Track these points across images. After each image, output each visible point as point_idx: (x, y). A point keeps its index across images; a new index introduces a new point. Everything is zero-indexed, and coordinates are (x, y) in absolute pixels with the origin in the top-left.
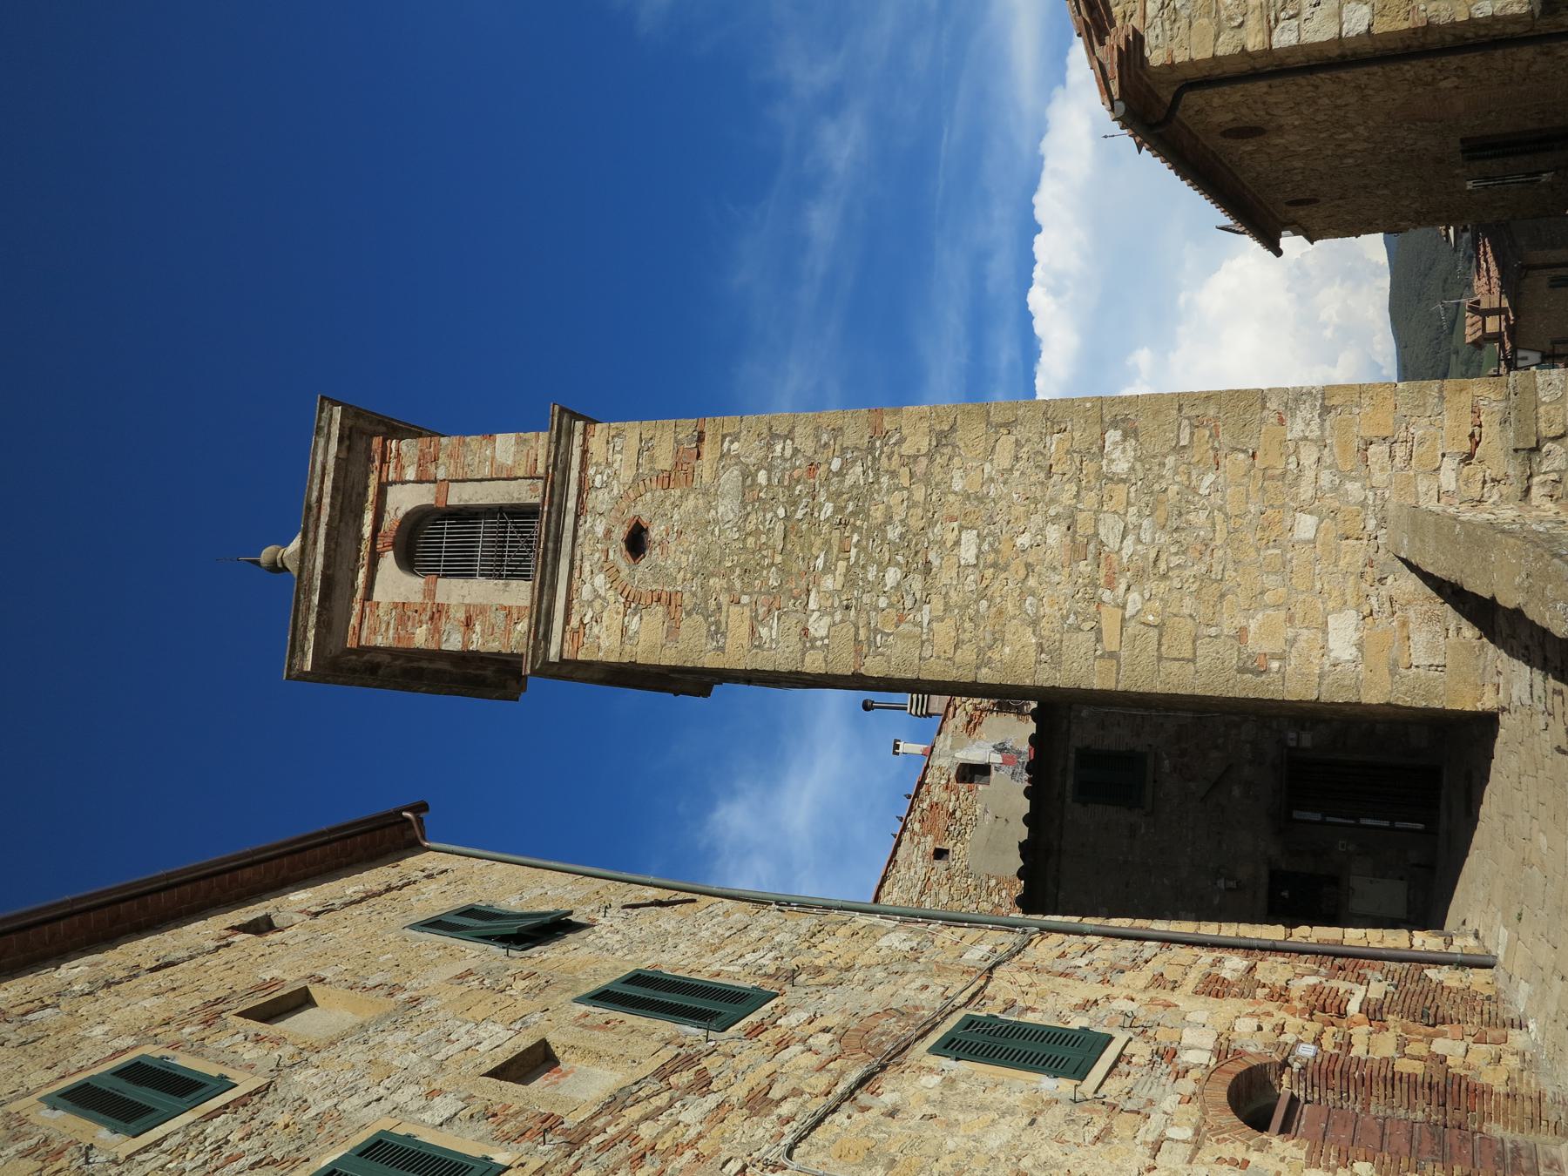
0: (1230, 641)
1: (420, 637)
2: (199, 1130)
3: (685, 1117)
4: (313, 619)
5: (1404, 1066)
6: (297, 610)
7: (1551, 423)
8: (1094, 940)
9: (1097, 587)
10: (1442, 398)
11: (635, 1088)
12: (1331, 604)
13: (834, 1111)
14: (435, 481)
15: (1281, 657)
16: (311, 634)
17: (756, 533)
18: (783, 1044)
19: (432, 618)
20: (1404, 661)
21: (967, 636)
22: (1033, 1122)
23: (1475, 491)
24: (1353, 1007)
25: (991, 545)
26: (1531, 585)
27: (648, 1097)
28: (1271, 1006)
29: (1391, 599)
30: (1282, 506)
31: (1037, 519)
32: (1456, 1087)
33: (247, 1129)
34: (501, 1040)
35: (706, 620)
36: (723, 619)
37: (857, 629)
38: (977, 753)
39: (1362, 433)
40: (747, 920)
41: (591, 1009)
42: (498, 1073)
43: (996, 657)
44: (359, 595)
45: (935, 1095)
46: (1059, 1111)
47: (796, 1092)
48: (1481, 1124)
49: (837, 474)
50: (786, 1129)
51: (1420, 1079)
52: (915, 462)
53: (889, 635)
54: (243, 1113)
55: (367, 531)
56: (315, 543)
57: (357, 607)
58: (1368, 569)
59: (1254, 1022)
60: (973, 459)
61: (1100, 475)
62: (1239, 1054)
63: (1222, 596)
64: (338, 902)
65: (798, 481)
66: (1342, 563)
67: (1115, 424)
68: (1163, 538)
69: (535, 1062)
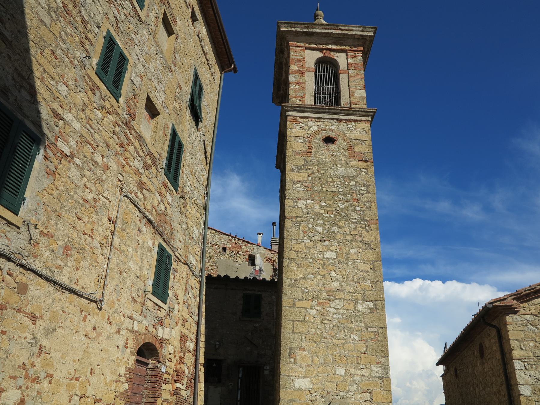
1: (293, 67)
4: (298, 30)
6: (301, 24)
9: (318, 299)
11: (145, 145)
12: (314, 379)
13: (139, 211)
14: (348, 69)
15: (295, 362)
16: (293, 29)
17: (333, 182)
18: (161, 194)
19: (300, 71)
22: (138, 277)
24: (178, 385)
25: (331, 263)
27: (142, 149)
28: (177, 358)
30: (347, 363)
31: (341, 279)
33: (127, 15)
34: (159, 100)
35: (302, 165)
36: (303, 171)
37: (301, 217)
40: (201, 182)
41: (170, 130)
42: (148, 99)
43: (292, 265)
44: (307, 45)
46: (142, 286)
47: (145, 199)
50: (133, 195)
52: (360, 236)
54: (132, 13)
55: (330, 47)
56: (325, 29)
57: (303, 45)
58: (326, 392)
59: (172, 352)
60: (361, 256)
63: (316, 342)
64: (203, 43)
65: (352, 195)
66: (328, 383)
67: (375, 305)
68: (335, 322)
69: (152, 111)
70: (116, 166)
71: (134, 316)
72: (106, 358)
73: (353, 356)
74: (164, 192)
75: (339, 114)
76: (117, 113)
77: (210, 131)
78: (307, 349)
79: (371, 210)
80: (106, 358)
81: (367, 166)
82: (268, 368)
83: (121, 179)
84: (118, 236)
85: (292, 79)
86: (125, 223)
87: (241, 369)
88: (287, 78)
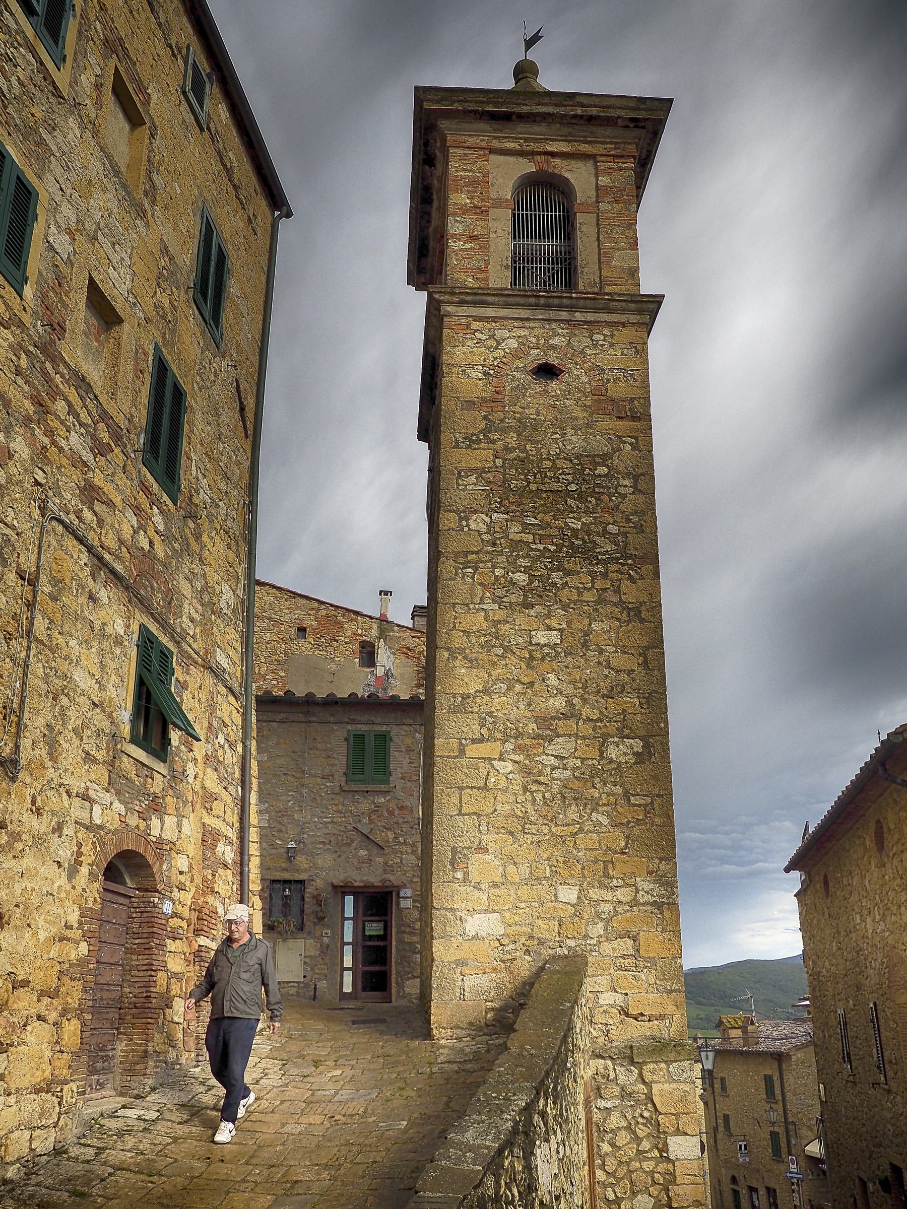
0: (476, 841)
2: (21, 42)
3: (74, 437)
5: (161, 978)
7: (653, 1072)
8: (240, 748)
9: (516, 738)
10: (671, 992)
11: (92, 396)
12: (508, 915)
13: (89, 551)
14: (597, 202)
15: (466, 880)
17: (554, 467)
18: (137, 510)
19: (476, 207)
20: (466, 970)
21: (473, 639)
22: (95, 705)
23: (600, 1018)
24: (203, 941)
25: (548, 654)
26: (524, 1057)
27: (86, 406)
28: (198, 880)
29: (515, 959)
30: (584, 876)
31: (569, 689)
32: (150, 1015)
33: (26, 83)
34: (118, 285)
35: (480, 432)
37: (477, 553)
38: (384, 657)
39: (642, 933)
40: (235, 479)
41: (151, 359)
42: (92, 285)
43: (457, 663)
45: (108, 630)
46: (105, 725)
47: (101, 522)
48: (124, 1034)
49: (605, 530)
50: (72, 516)
51: (153, 989)
52: (615, 591)
53: (473, 578)
54: (39, 78)
58: (536, 942)
59: (185, 869)
60: (617, 637)
61: (606, 736)
62: (160, 858)
63: (511, 833)
64: (221, 146)
65: (598, 499)
66: (540, 922)
67: (647, 746)
68: (556, 788)
69: (104, 312)
70: (26, 450)
71: (91, 792)
72: (33, 889)
73: (597, 861)
74: (145, 505)
75: (571, 308)
76: (21, 324)
77: (252, 358)
78: (492, 847)
79: (643, 532)
80: (33, 889)
81: (636, 430)
82: (409, 893)
83: (43, 481)
84: (43, 612)
85: (455, 227)
86: (56, 582)
87: (349, 900)
88: (444, 224)
